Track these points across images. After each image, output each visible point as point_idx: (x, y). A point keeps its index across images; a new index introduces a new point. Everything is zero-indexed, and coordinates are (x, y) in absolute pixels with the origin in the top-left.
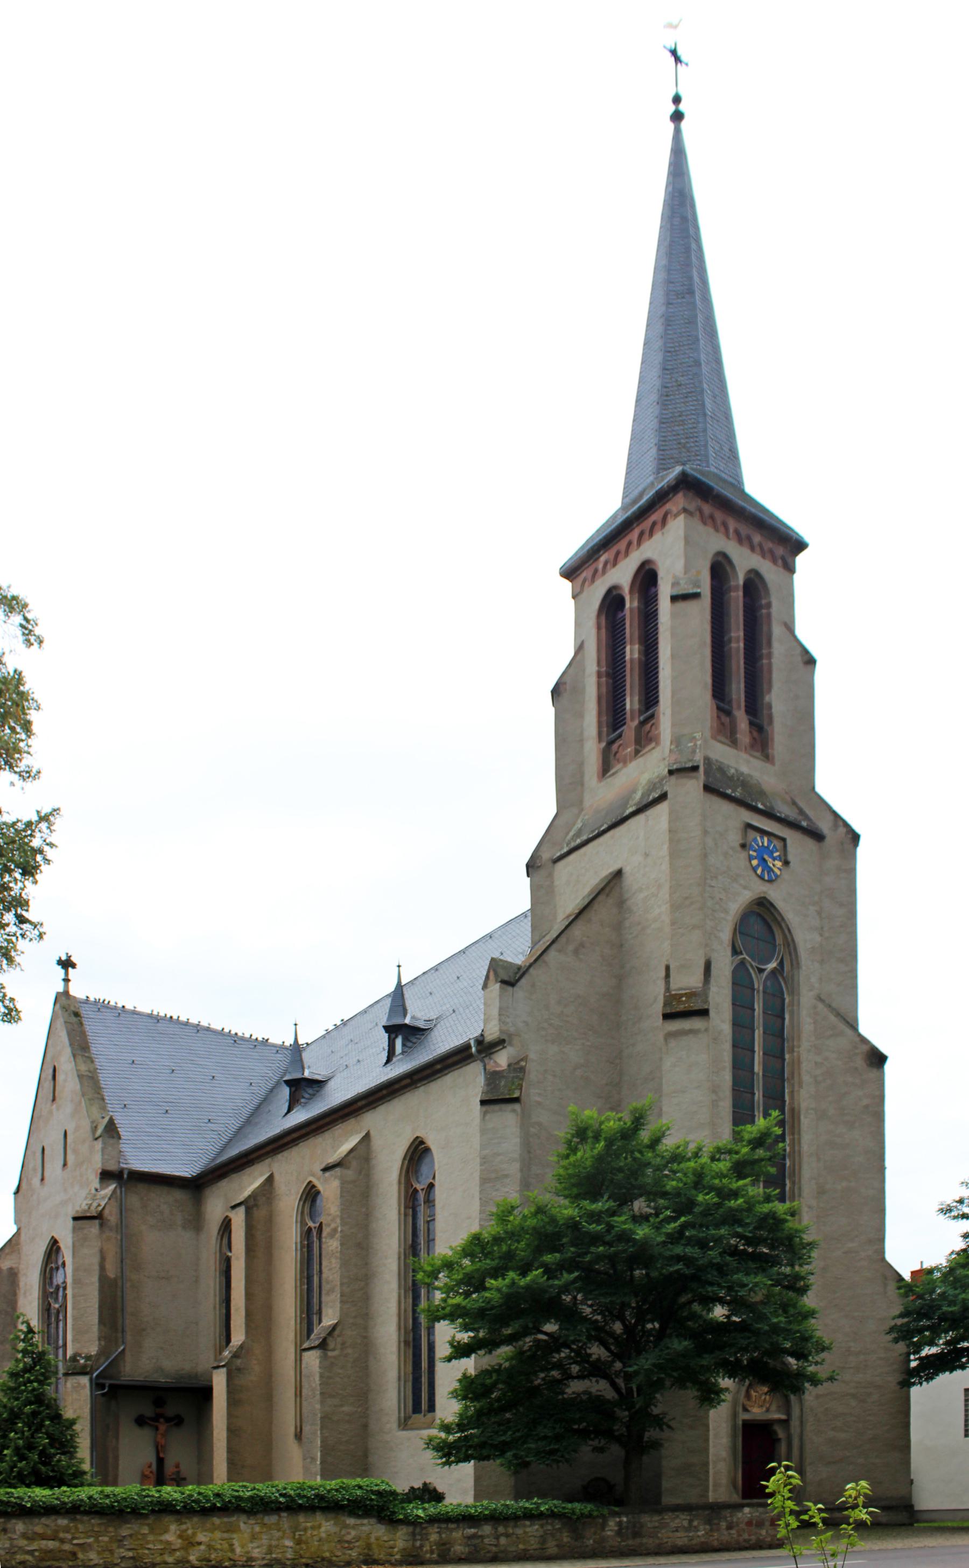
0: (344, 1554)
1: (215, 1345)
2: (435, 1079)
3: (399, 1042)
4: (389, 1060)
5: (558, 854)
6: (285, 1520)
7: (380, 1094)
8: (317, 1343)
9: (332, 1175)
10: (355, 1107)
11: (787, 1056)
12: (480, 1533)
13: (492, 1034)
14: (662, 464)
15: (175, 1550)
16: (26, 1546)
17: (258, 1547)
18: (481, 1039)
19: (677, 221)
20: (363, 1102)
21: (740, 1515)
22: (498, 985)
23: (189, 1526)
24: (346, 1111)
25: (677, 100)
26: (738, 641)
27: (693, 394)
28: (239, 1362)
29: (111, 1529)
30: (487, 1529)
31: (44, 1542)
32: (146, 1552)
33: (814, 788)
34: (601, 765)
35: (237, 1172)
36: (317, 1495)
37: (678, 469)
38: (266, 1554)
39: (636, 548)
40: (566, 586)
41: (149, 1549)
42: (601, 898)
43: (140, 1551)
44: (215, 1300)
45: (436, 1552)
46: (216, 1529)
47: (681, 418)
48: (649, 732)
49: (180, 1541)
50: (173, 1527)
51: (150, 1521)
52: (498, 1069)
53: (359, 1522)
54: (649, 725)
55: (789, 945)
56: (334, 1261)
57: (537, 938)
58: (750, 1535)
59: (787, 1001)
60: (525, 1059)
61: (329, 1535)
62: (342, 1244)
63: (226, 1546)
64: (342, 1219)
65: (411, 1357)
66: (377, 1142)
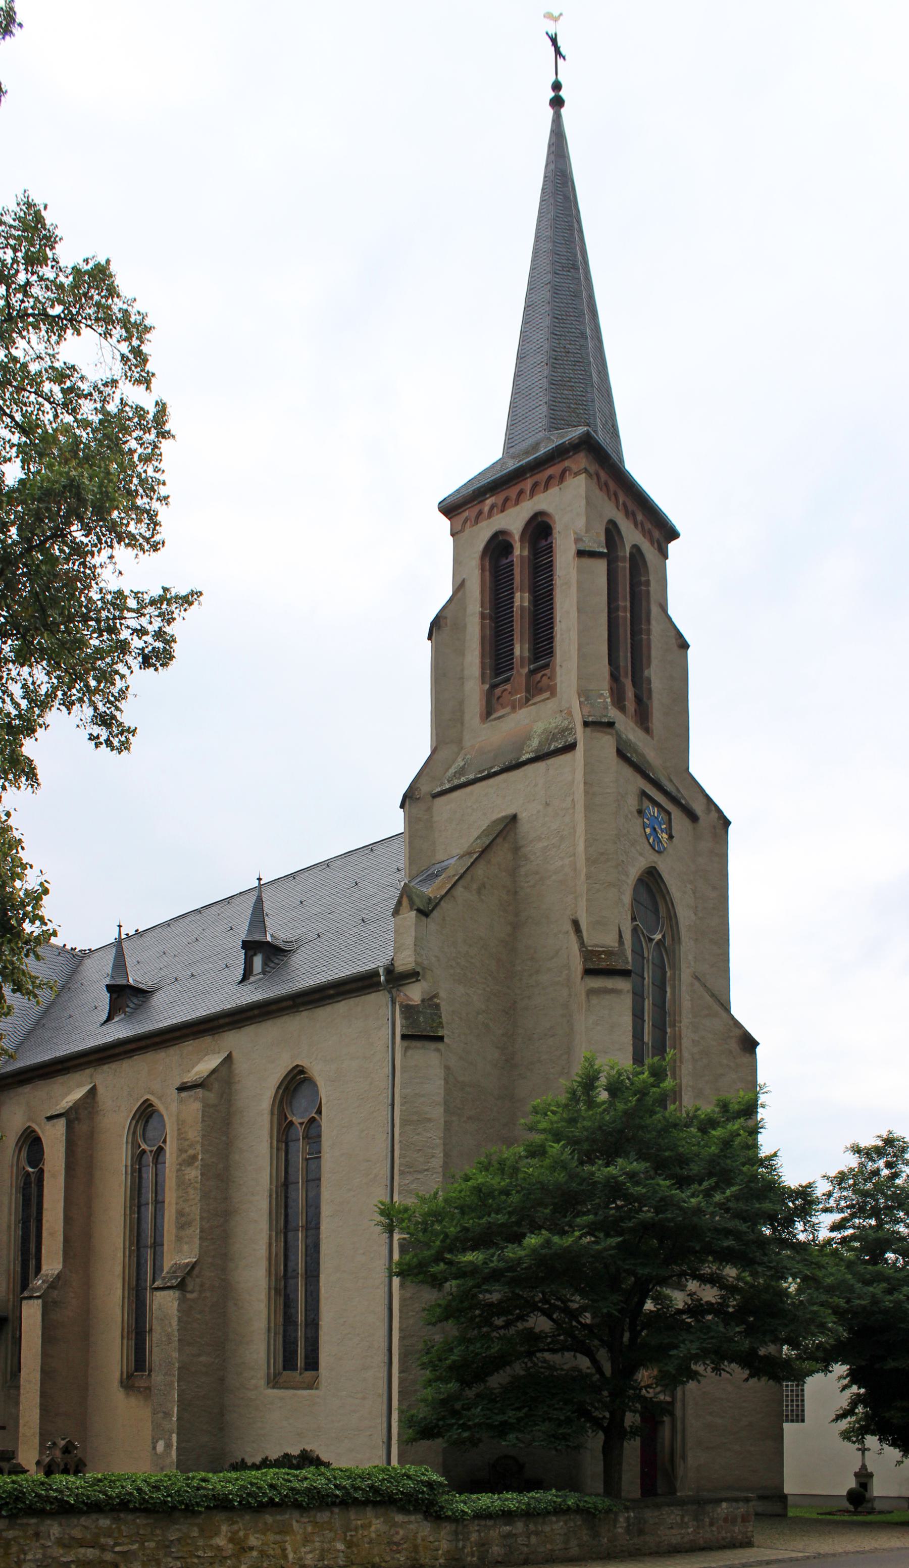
0: (393, 1558)
1: (9, 1270)
2: (323, 1006)
3: (258, 961)
4: (245, 978)
5: (439, 789)
6: (336, 1517)
7: (250, 1014)
8: (174, 1282)
9: (190, 1097)
10: (216, 1023)
11: (669, 1030)
12: (514, 1532)
13: (406, 962)
14: (555, 423)
15: (226, 1558)
16: (62, 1556)
17: (310, 1552)
18: (391, 968)
19: (560, 198)
20: (227, 1020)
21: (719, 1510)
22: (413, 913)
23: (241, 1524)
24: (202, 1027)
25: (557, 86)
26: (625, 611)
27: (581, 364)
28: (55, 1293)
29: (158, 1532)
30: (519, 1526)
31: (82, 1550)
32: (196, 1561)
33: (688, 768)
34: (484, 707)
35: (44, 1079)
36: (372, 1487)
37: (581, 430)
38: (319, 1561)
39: (528, 498)
40: (445, 524)
41: (199, 1557)
42: (499, 840)
43: (188, 1560)
44: (10, 1220)
45: (476, 1553)
46: (268, 1530)
47: (569, 384)
48: (539, 682)
49: (231, 1546)
50: (224, 1528)
51: (199, 1520)
52: (411, 1003)
53: (406, 1519)
54: (540, 674)
55: (671, 920)
56: (191, 1191)
57: (414, 872)
58: (726, 1533)
59: (668, 974)
60: (436, 996)
61: (378, 1535)
62: (202, 1174)
63: (278, 1551)
64: (203, 1145)
65: (282, 1307)
66: (241, 1065)
